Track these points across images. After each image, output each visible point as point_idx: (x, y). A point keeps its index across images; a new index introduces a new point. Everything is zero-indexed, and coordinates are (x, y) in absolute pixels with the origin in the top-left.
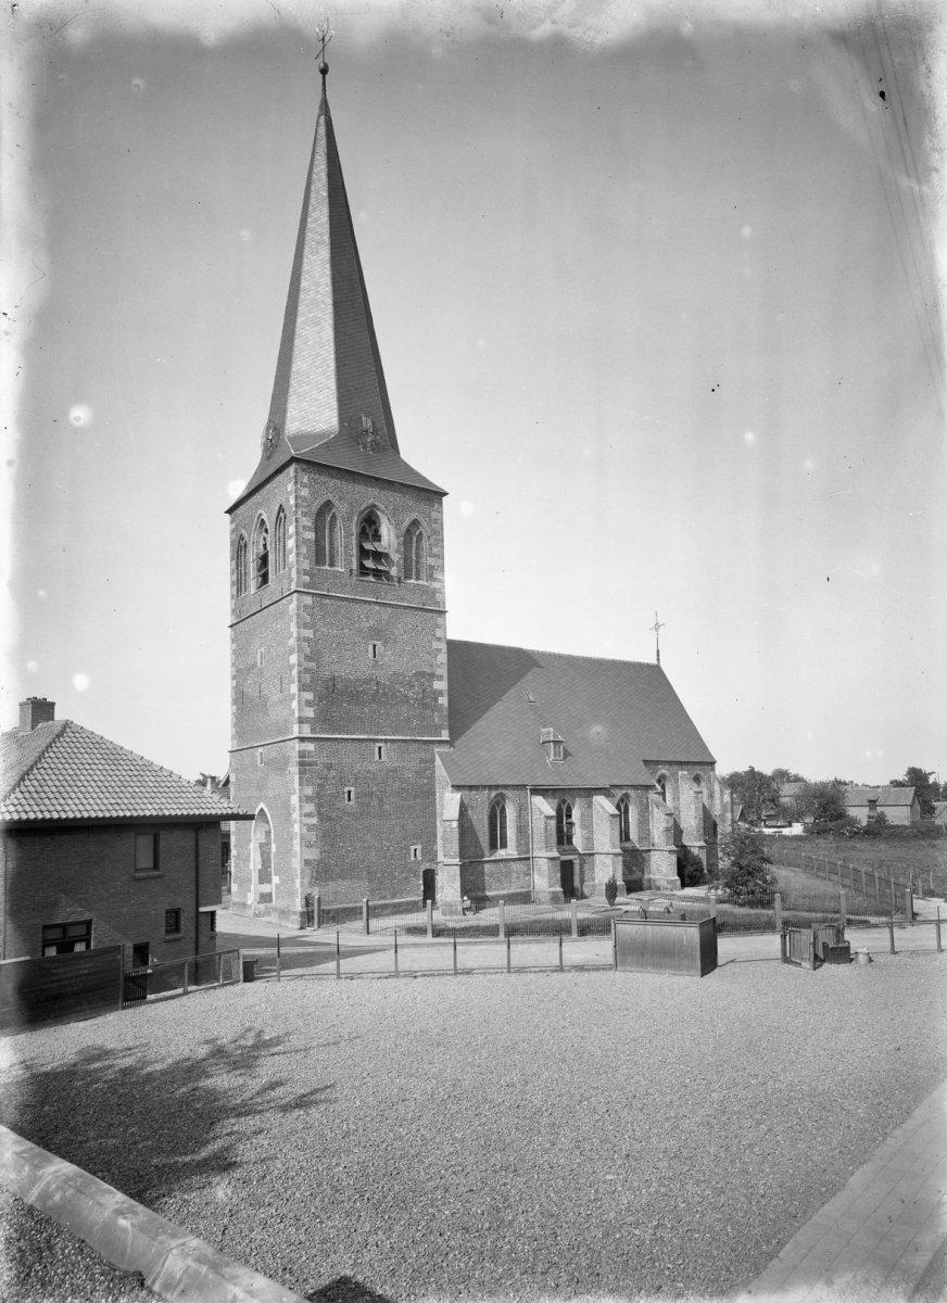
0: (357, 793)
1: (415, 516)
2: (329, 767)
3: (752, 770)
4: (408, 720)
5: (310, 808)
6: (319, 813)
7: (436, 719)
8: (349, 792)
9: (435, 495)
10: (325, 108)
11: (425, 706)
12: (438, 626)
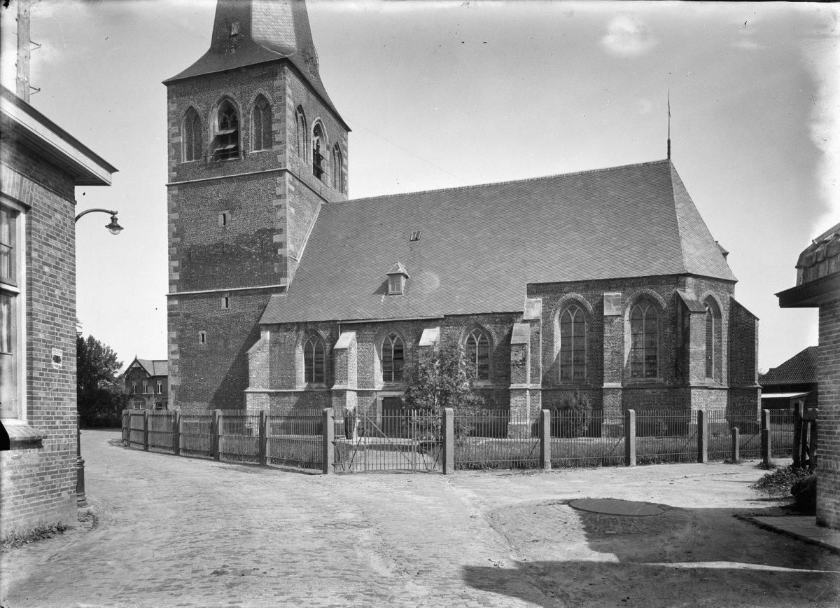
0: (208, 336)
1: (256, 93)
2: (188, 316)
3: (796, 267)
4: (251, 272)
5: (175, 347)
6: (181, 352)
7: (276, 269)
8: (203, 335)
9: (348, 130)
10: (669, 141)
11: (265, 259)
12: (278, 185)
